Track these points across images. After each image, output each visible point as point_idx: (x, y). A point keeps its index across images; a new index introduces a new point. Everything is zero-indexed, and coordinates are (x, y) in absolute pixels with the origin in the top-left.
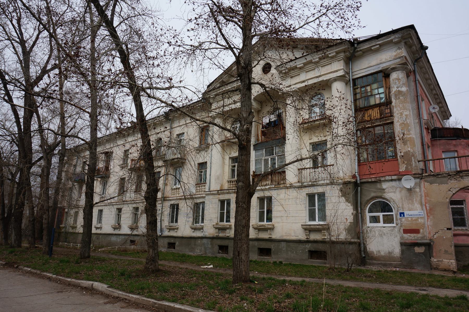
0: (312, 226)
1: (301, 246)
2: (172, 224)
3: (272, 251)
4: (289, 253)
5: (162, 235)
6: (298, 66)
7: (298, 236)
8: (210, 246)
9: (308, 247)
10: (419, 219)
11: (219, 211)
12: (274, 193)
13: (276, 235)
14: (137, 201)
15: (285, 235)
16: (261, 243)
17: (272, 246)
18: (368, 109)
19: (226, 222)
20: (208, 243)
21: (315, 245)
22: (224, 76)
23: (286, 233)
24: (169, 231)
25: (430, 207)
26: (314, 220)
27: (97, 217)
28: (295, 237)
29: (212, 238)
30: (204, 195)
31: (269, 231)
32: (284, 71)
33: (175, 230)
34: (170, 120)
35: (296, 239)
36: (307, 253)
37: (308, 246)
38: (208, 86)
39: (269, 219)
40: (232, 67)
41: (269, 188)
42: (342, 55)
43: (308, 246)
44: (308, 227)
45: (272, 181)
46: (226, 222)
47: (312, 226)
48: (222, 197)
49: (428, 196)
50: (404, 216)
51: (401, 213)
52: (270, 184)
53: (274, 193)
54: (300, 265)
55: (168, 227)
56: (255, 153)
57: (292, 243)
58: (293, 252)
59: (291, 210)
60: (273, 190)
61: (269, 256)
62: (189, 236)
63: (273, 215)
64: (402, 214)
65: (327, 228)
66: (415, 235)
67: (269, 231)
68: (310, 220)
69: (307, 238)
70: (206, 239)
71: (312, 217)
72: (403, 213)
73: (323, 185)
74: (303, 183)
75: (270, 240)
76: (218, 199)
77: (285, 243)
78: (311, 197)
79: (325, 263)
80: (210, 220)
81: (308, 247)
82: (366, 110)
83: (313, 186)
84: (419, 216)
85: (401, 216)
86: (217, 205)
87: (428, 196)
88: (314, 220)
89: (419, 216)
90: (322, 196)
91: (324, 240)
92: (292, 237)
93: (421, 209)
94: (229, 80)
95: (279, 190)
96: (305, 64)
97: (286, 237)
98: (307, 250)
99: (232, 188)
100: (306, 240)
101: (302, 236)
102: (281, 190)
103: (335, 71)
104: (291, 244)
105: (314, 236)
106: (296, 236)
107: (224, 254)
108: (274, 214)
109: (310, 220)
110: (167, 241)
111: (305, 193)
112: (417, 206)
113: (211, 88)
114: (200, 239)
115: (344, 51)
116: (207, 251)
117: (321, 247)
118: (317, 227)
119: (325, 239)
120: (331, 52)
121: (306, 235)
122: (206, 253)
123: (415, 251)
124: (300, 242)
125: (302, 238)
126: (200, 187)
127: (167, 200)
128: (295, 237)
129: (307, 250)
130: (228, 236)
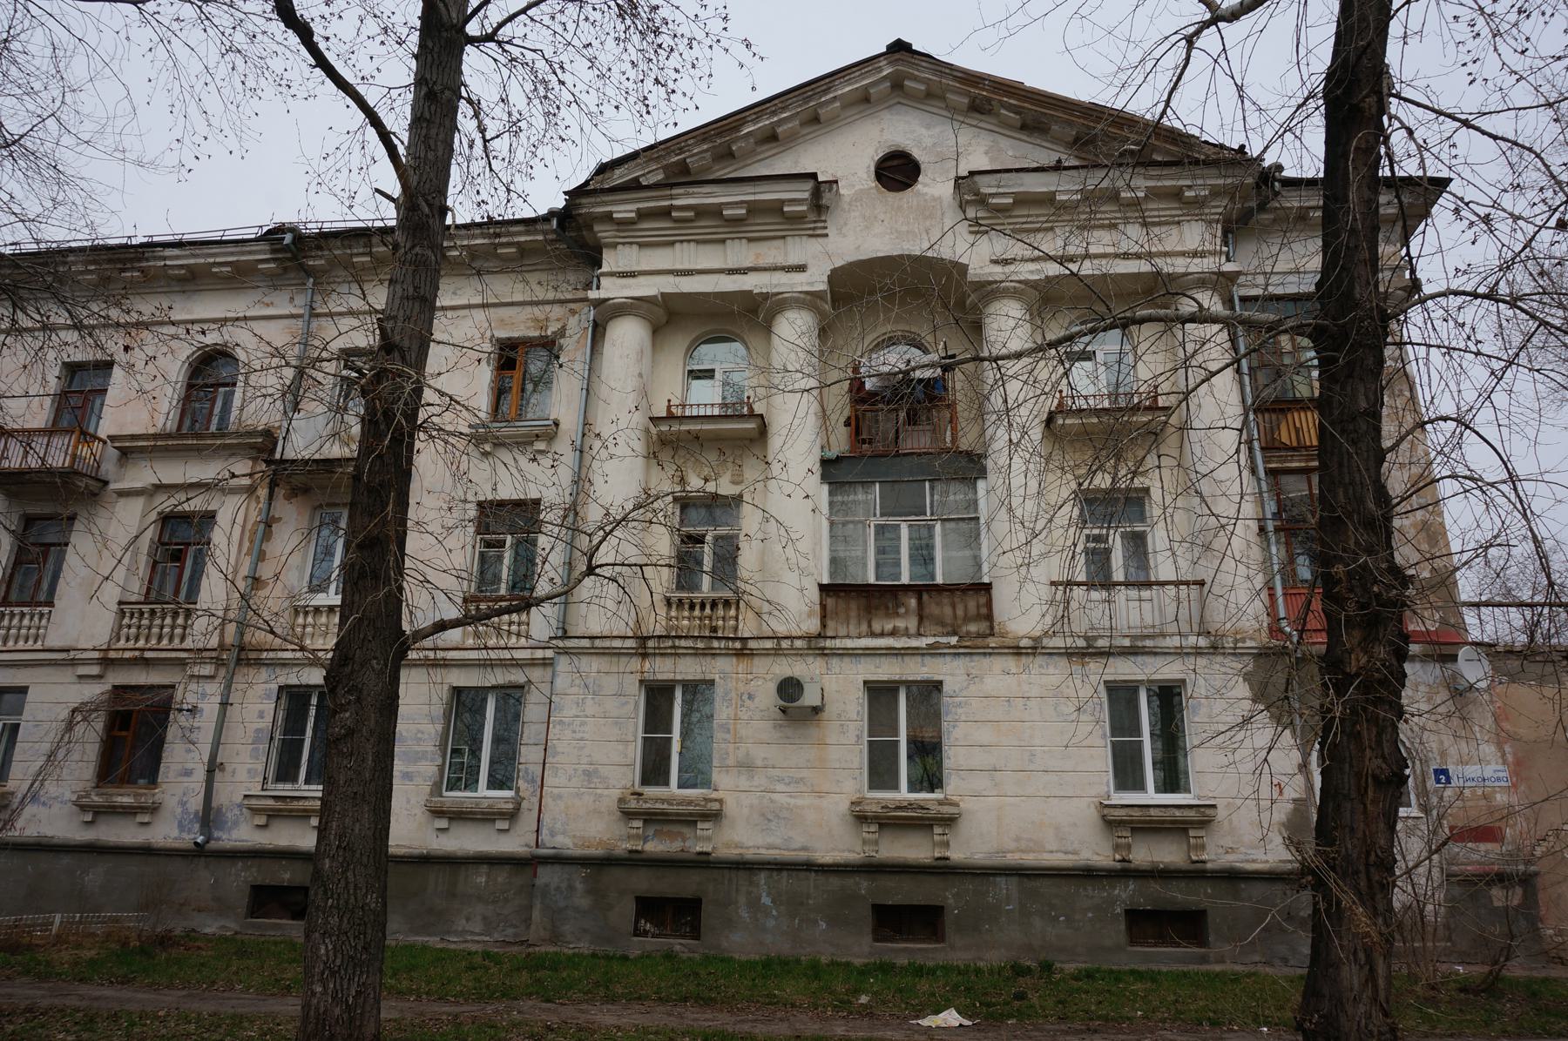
0: (1153, 812)
1: (1093, 894)
2: (284, 789)
3: (948, 920)
4: (1037, 922)
5: (213, 845)
6: (615, 216)
7: (1075, 853)
8: (584, 902)
9: (1124, 896)
10: (1496, 792)
11: (640, 734)
12: (950, 672)
13: (967, 847)
14: (518, 654)
15: (1012, 845)
16: (889, 882)
17: (950, 896)
18: (1289, 409)
19: (680, 786)
20: (571, 888)
21: (1155, 887)
22: (696, 145)
23: (1018, 839)
24: (265, 827)
25: (1515, 754)
26: (1140, 786)
27: (433, 730)
28: (1061, 856)
29: (599, 865)
30: (549, 653)
31: (937, 830)
32: (1192, 194)
33: (140, 818)
34: (309, 272)
35: (1070, 864)
36: (1122, 919)
37: (1125, 893)
38: (603, 169)
39: (930, 779)
40: (744, 122)
41: (930, 646)
42: (1218, 207)
43: (1125, 893)
44: (1136, 813)
45: (921, 619)
46: (680, 786)
47: (1153, 812)
48: (663, 669)
49: (1507, 719)
50: (1448, 780)
51: (1438, 772)
52: (913, 629)
53: (950, 672)
54: (1089, 975)
55: (271, 802)
56: (831, 493)
57: (1046, 882)
58: (1056, 918)
59: (1037, 742)
60: (948, 659)
61: (938, 941)
62: (416, 852)
63: (947, 763)
64: (1442, 773)
65: (1199, 821)
66: (1489, 846)
67: (937, 830)
68: (872, 787)
69: (1123, 860)
70: (557, 868)
71: (1127, 771)
72: (1445, 772)
73: (1180, 652)
74: (1095, 638)
75: (943, 870)
76: (638, 676)
77: (1015, 880)
78: (1121, 696)
79: (1204, 960)
80: (587, 773)
81: (1124, 896)
82: (1282, 410)
83: (1132, 652)
84: (1497, 784)
85: (1438, 781)
86: (631, 707)
87: (1507, 719)
88: (1140, 786)
89: (1497, 784)
90: (1169, 697)
91: (1199, 866)
92: (1046, 856)
93: (1500, 761)
94: (708, 169)
95: (976, 658)
96: (643, 215)
97: (1017, 856)
98: (1119, 910)
99: (171, 639)
100: (1118, 866)
101: (1096, 851)
102: (986, 661)
103: (681, 271)
104: (1044, 886)
105: (1145, 853)
106: (1066, 853)
107: (666, 936)
108: (953, 757)
109: (872, 787)
110: (239, 879)
111: (861, 679)
112: (1488, 750)
113: (620, 176)
114: (484, 869)
115: (1230, 192)
116: (567, 928)
117: (1179, 896)
118: (1178, 813)
119: (1203, 862)
120: (1196, 185)
121: (865, 842)
122: (555, 937)
123: (1492, 902)
124: (1087, 874)
125: (1096, 858)
126: (23, 615)
127: (259, 663)
128: (1061, 856)
129: (1119, 910)
130: (700, 853)
